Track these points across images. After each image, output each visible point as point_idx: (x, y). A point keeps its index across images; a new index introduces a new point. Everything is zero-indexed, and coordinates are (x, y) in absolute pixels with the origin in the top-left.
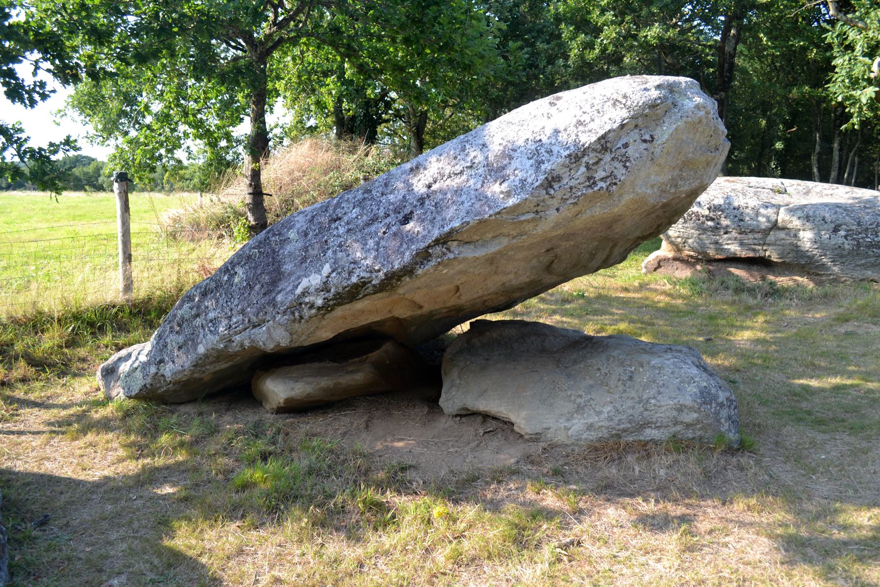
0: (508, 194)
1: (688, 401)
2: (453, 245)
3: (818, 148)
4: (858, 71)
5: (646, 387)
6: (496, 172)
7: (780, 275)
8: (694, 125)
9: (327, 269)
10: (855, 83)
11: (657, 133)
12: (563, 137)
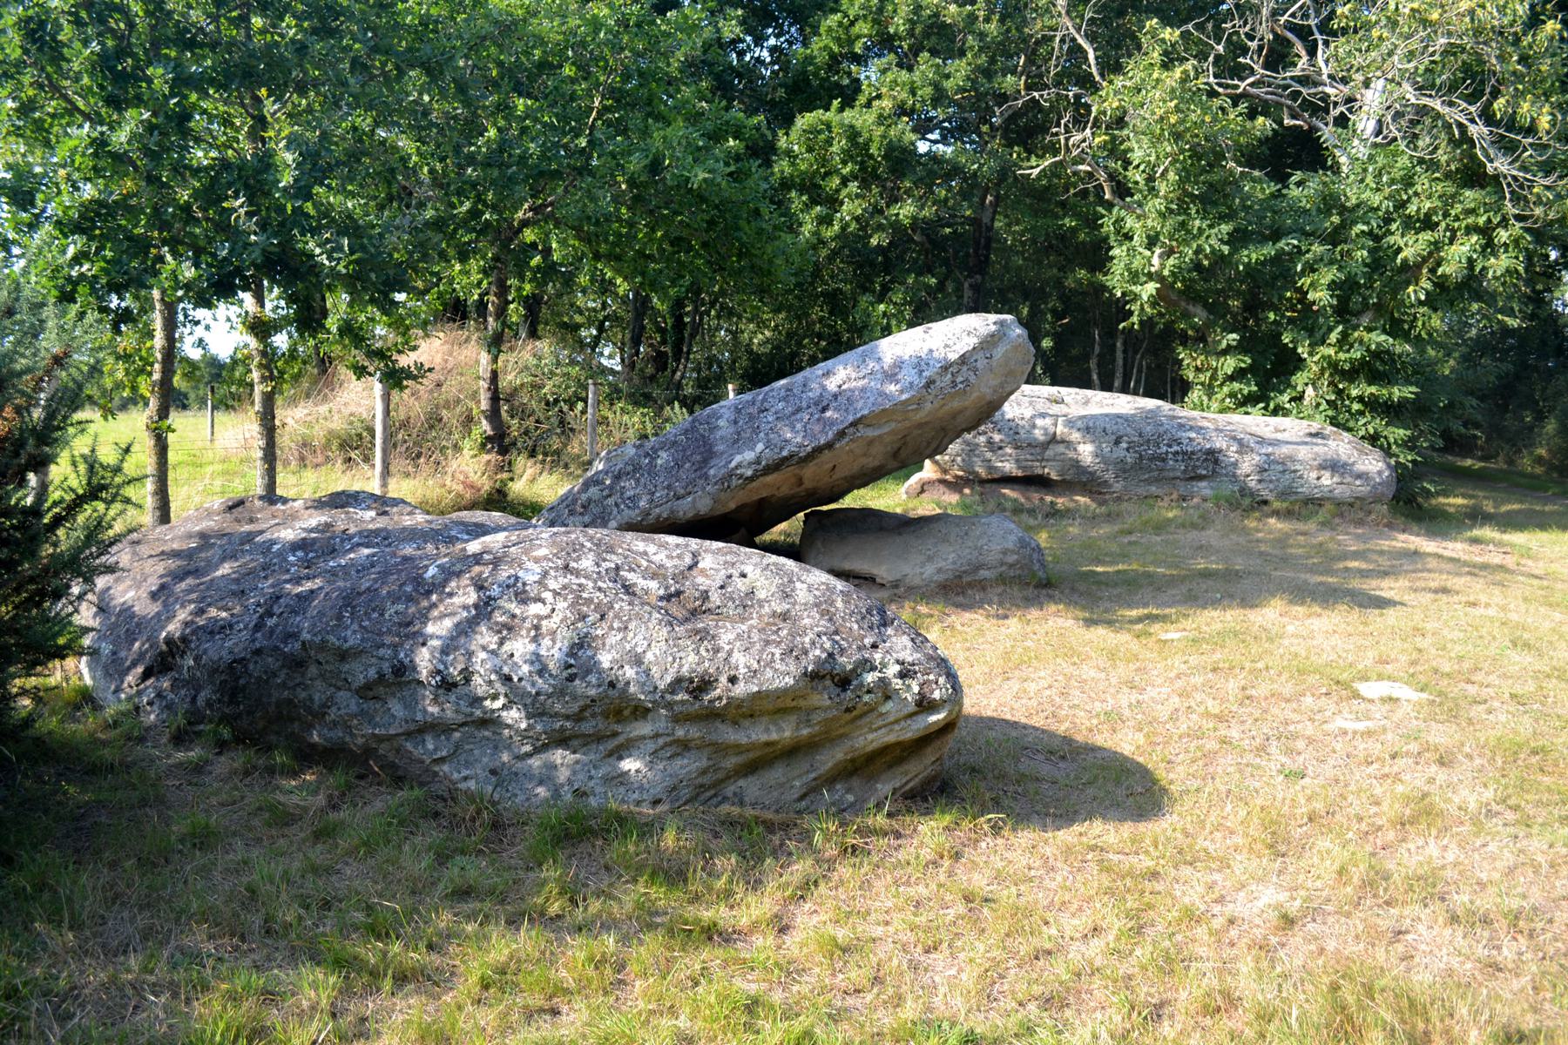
0: (902, 392)
1: (1010, 545)
2: (860, 427)
3: (1097, 349)
4: (1137, 264)
5: (979, 538)
6: (891, 376)
7: (1060, 495)
8: (1016, 348)
9: (760, 447)
10: (1134, 277)
11: (994, 353)
12: (936, 354)
